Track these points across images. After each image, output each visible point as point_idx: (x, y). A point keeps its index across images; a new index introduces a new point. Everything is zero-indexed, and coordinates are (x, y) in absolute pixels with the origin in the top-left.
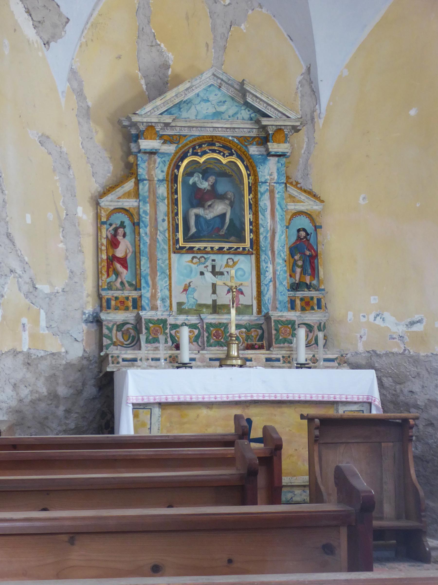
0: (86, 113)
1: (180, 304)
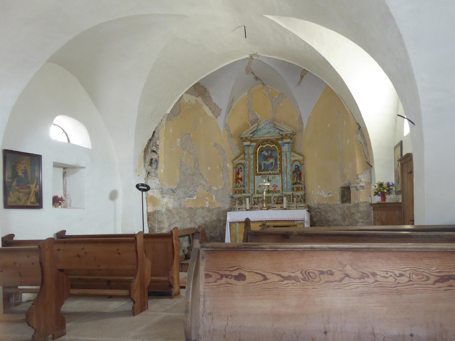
0: (231, 136)
1: (257, 191)
